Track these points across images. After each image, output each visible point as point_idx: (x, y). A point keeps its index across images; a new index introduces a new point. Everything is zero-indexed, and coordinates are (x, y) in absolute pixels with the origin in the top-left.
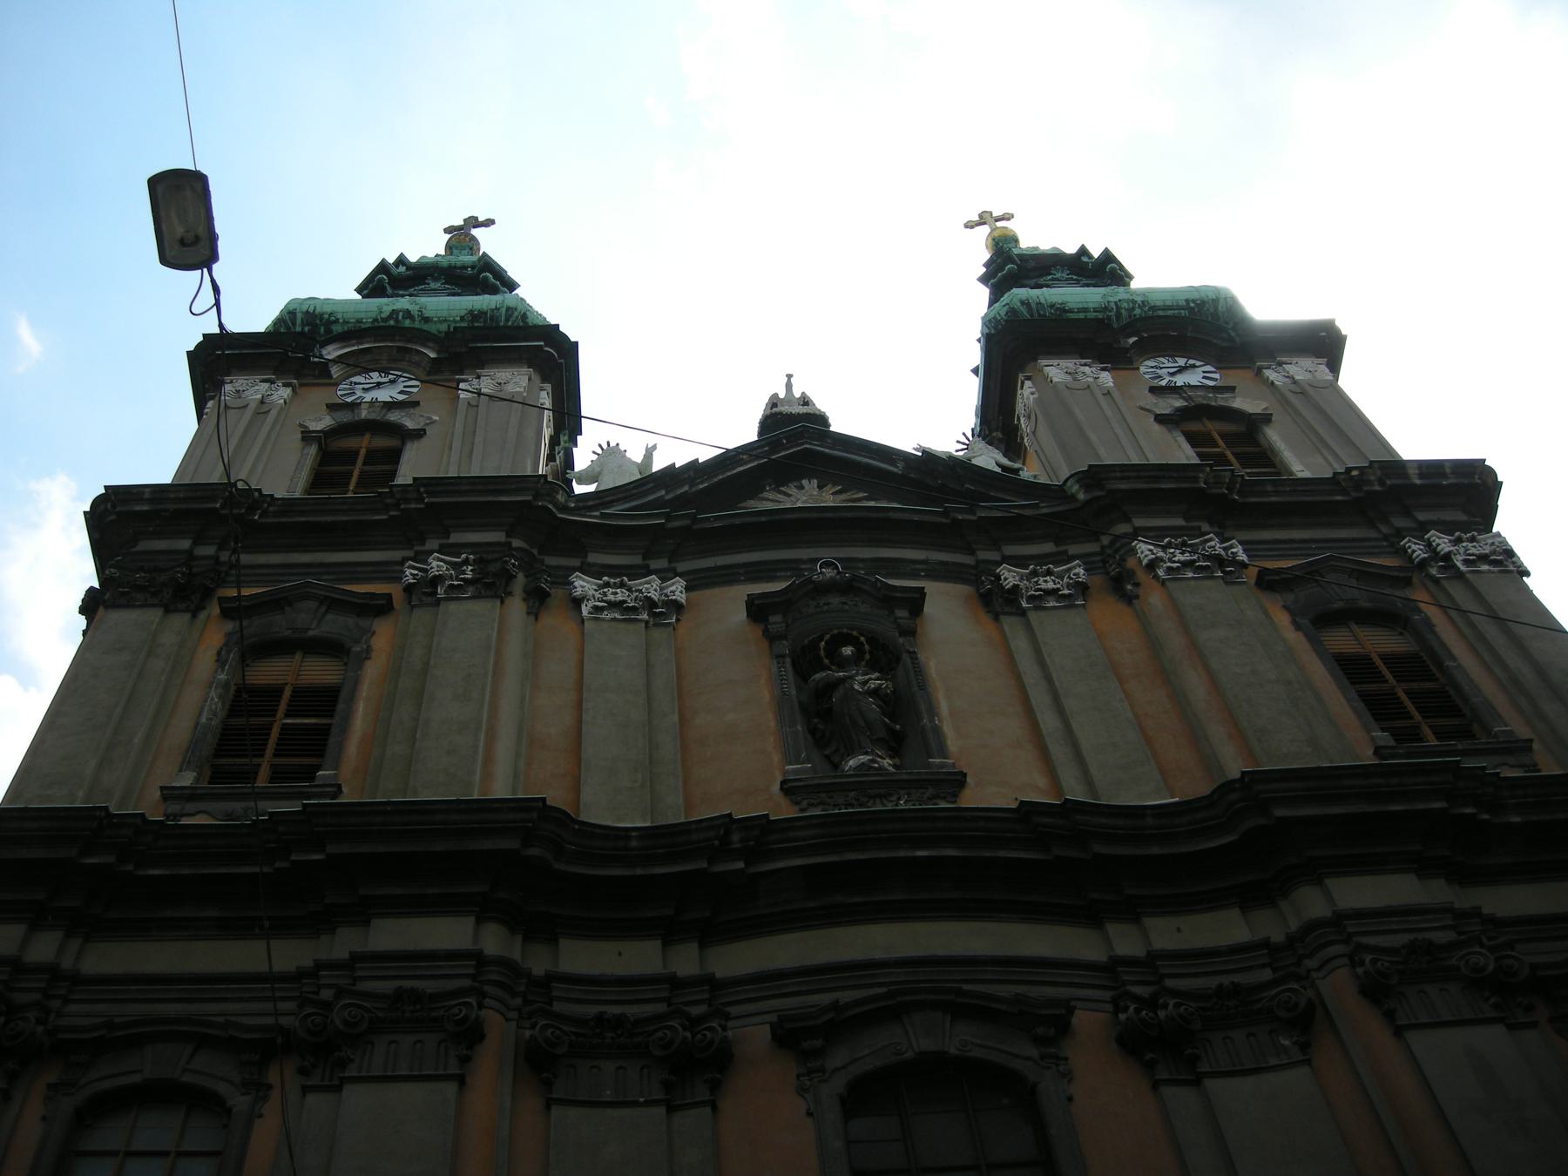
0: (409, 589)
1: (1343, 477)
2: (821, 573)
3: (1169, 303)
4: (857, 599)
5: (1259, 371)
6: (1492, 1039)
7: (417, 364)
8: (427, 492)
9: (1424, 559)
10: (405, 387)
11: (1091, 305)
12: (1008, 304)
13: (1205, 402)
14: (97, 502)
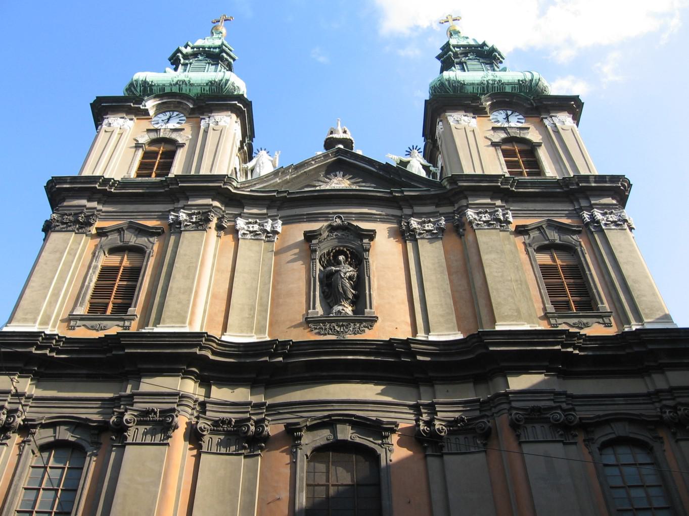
0: (170, 225)
1: (561, 181)
2: (336, 221)
3: (510, 81)
4: (348, 233)
5: (542, 120)
6: (556, 449)
7: (185, 109)
8: (180, 181)
9: (588, 222)
10: (180, 120)
11: (476, 82)
12: (440, 80)
13: (515, 135)
14: (48, 183)
